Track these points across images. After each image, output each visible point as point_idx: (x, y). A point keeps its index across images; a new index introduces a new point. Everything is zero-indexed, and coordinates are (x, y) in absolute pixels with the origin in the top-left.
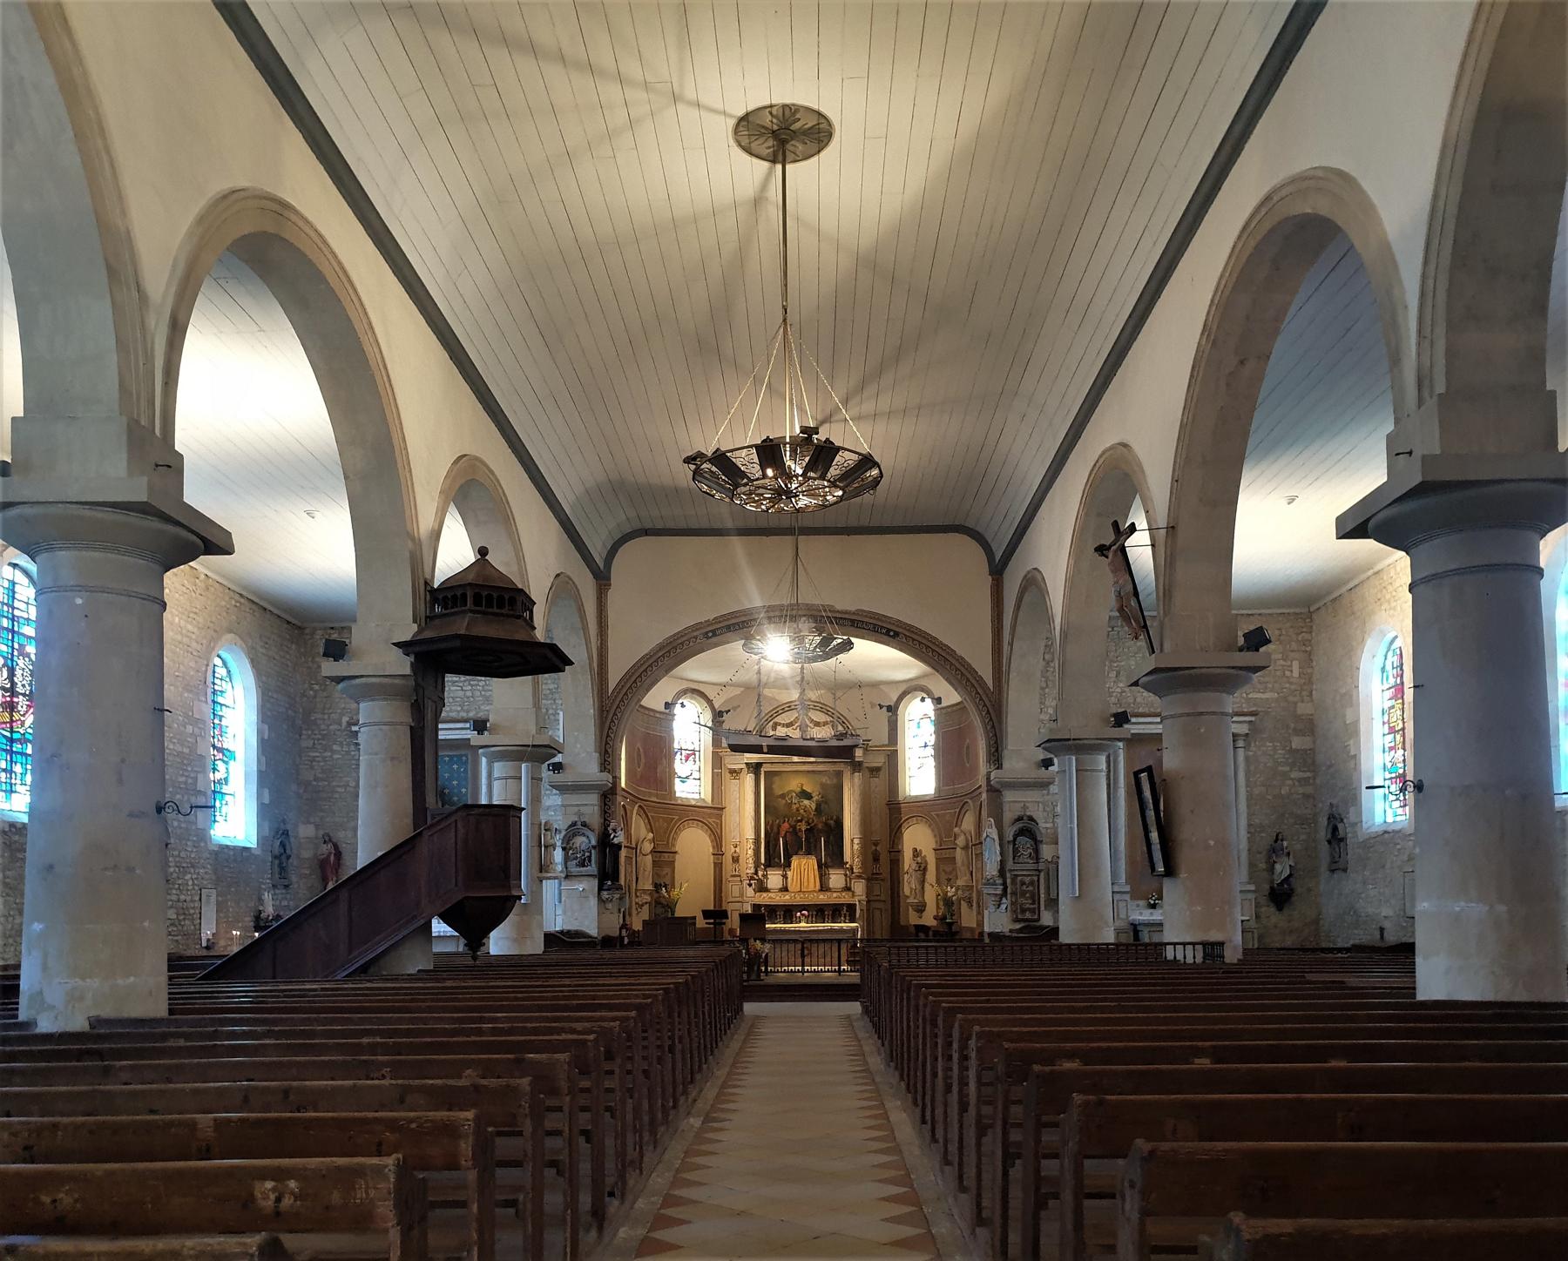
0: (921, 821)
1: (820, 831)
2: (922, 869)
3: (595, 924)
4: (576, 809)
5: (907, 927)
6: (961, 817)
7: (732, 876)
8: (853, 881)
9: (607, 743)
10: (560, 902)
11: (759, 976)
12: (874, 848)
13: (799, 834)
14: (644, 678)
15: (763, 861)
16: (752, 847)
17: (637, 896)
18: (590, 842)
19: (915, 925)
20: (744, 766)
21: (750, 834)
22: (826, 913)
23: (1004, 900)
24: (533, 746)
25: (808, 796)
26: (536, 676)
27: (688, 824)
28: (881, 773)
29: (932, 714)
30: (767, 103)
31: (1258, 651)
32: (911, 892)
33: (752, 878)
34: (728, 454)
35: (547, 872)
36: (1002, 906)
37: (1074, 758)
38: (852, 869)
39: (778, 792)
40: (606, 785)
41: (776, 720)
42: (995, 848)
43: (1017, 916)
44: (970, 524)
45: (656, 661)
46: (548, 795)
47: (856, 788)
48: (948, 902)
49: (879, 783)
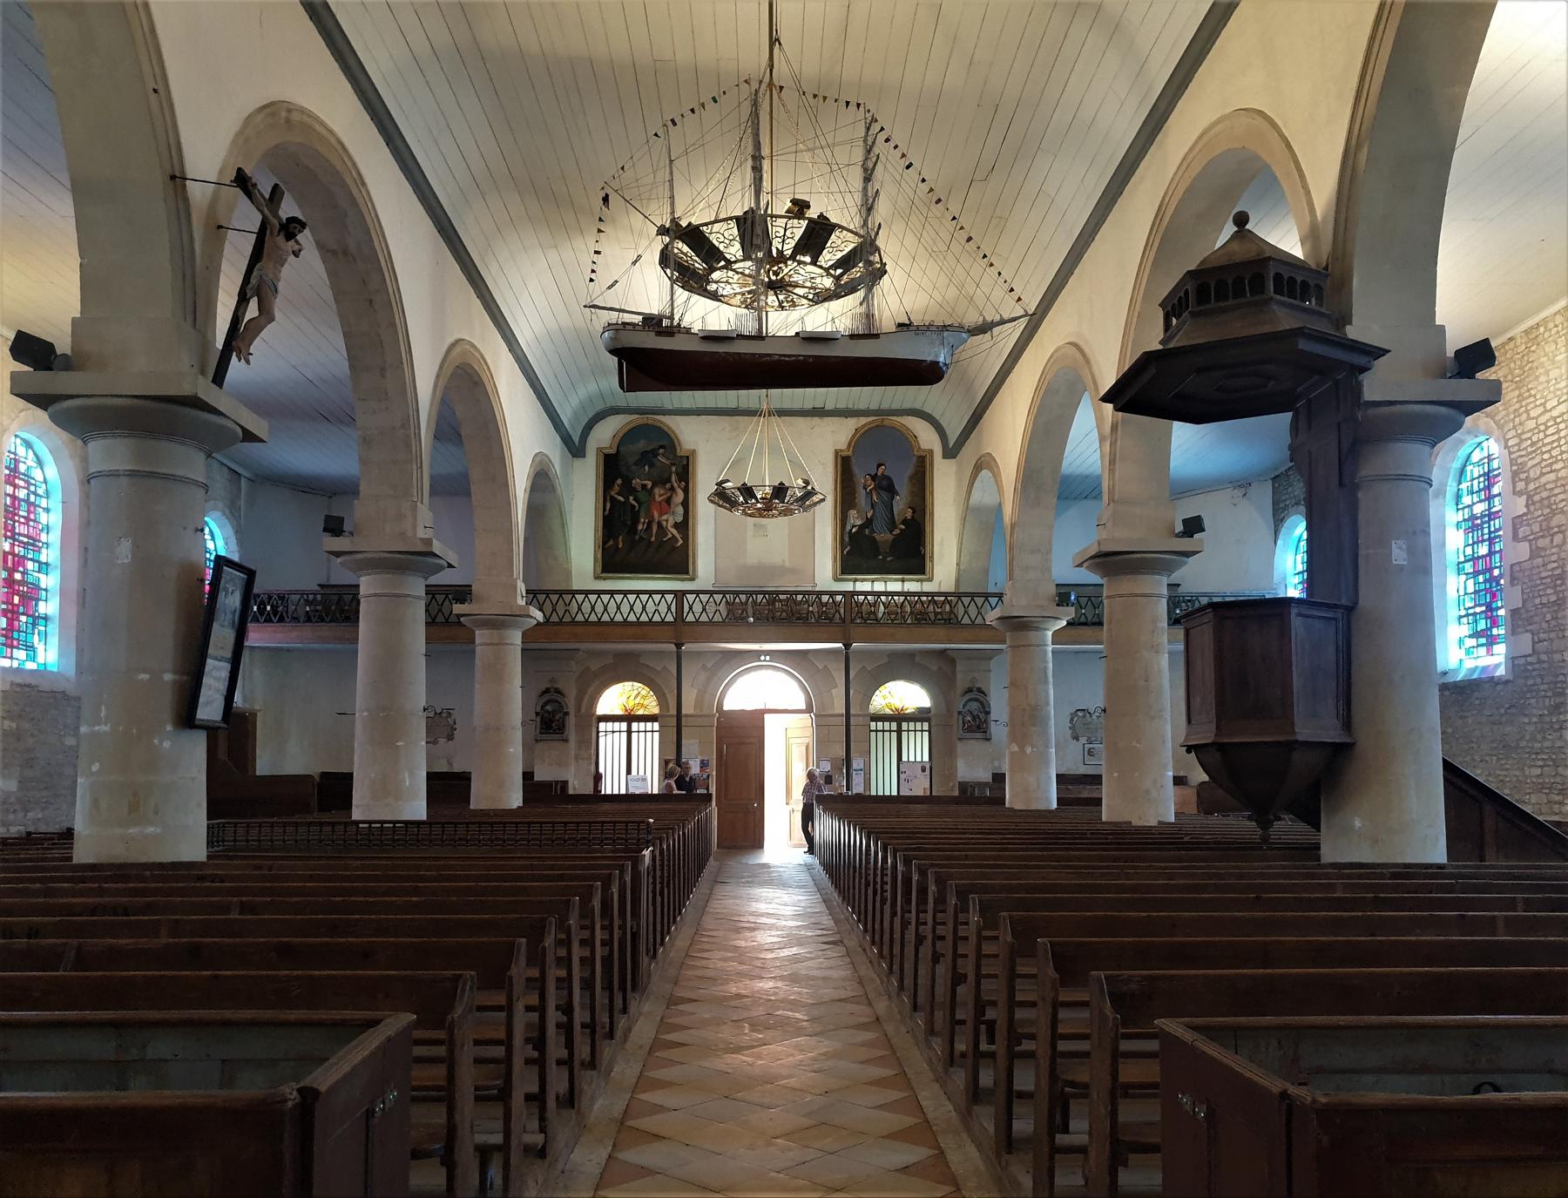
31: (1192, 537)
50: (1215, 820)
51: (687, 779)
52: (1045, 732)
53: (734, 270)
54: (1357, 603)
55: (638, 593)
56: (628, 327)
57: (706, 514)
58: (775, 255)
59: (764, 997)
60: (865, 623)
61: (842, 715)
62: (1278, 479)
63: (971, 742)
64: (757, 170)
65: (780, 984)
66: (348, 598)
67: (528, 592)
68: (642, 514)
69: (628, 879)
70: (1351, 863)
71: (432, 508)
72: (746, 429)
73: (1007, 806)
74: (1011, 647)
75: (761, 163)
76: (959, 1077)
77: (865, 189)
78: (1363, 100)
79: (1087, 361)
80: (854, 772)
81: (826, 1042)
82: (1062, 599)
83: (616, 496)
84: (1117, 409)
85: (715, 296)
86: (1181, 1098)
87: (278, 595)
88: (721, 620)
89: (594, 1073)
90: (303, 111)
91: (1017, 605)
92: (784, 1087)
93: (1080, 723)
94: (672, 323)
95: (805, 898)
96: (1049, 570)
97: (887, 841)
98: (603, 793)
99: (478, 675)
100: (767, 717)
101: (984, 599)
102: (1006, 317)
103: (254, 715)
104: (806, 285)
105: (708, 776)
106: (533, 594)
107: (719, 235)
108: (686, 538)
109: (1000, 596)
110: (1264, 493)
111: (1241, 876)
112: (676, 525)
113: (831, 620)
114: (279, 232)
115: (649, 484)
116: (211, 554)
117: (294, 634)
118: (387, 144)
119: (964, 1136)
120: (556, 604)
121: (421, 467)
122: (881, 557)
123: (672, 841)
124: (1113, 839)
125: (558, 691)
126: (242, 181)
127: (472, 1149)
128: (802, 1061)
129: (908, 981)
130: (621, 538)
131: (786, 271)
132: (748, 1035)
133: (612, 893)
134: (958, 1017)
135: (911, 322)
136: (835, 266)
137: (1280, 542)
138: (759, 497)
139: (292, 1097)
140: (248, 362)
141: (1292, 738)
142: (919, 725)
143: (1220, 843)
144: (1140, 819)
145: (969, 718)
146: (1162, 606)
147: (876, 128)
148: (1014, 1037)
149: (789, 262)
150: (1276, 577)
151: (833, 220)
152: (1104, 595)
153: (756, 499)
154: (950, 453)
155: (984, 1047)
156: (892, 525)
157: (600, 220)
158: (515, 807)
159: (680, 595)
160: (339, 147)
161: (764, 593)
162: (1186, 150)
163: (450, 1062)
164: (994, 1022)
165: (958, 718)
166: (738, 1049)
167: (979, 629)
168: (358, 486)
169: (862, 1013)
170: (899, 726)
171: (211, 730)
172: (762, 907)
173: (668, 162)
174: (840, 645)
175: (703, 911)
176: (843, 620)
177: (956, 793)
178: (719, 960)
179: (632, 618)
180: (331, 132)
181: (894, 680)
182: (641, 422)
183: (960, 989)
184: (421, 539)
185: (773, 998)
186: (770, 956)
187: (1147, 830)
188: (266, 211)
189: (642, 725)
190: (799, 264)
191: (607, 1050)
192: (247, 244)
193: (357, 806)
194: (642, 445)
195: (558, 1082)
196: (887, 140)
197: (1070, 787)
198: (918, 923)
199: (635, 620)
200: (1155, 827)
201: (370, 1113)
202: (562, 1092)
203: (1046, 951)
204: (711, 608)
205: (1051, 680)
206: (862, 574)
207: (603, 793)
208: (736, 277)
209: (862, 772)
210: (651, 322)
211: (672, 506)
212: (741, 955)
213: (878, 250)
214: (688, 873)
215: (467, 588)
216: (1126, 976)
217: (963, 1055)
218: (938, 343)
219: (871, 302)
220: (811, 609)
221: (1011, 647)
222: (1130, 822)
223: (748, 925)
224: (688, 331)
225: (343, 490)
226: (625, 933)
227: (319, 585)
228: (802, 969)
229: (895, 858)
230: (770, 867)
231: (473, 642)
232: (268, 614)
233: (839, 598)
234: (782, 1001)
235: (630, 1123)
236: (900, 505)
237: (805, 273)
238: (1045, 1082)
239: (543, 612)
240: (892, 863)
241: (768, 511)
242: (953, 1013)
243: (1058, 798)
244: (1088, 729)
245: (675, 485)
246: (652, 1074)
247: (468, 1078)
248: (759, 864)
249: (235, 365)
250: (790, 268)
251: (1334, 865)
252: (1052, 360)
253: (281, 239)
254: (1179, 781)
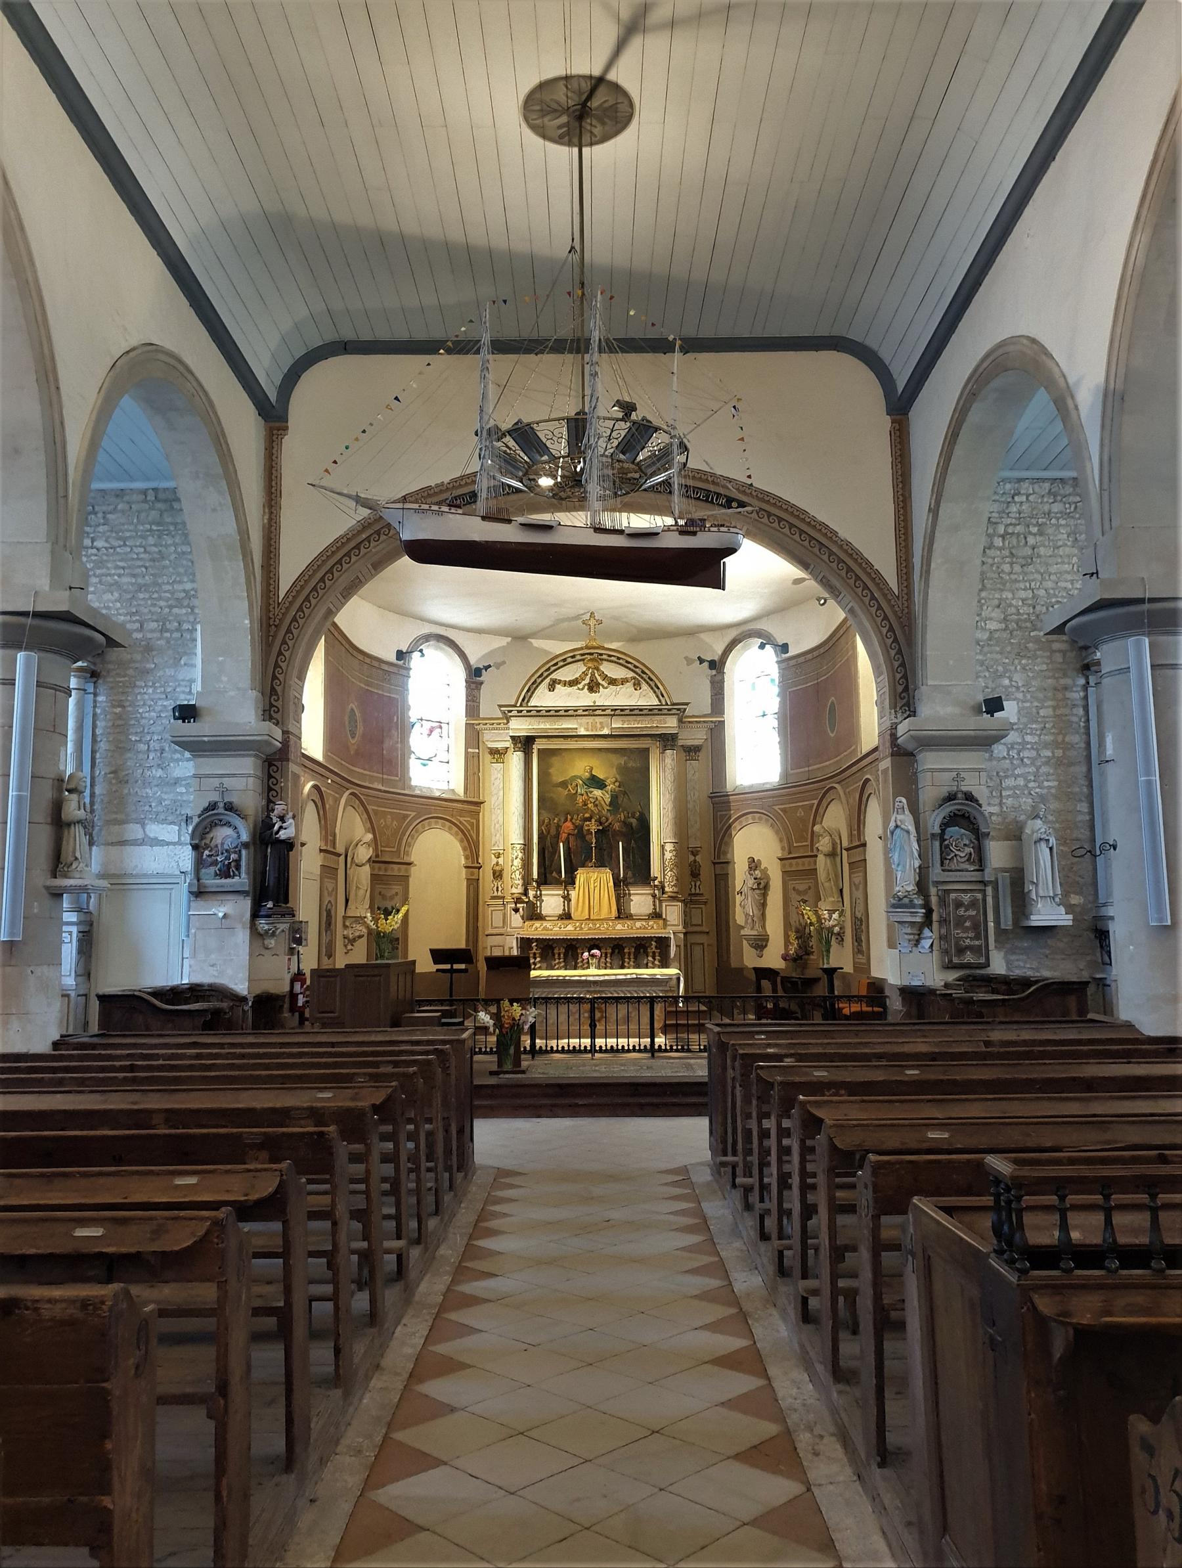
0: (760, 819)
1: (615, 833)
2: (762, 887)
3: (243, 974)
4: (216, 782)
5: (741, 970)
6: (821, 810)
7: (493, 898)
8: (664, 904)
9: (274, 677)
10: (188, 936)
11: (517, 1062)
12: (692, 858)
13: (588, 838)
14: (336, 574)
15: (535, 876)
16: (520, 855)
17: (345, 927)
18: (239, 837)
19: (755, 969)
20: (508, 744)
21: (515, 836)
22: (626, 950)
23: (927, 933)
24: (37, 615)
25: (599, 783)
27: (429, 824)
28: (702, 755)
29: (774, 671)
32: (746, 922)
33: (518, 901)
35: (66, 876)
36: (923, 941)
37: (1147, 640)
38: (663, 888)
39: (558, 778)
40: (267, 743)
41: (553, 676)
42: (910, 846)
43: (950, 961)
44: (855, 335)
45: (357, 547)
46: (178, 760)
47: (668, 772)
48: (802, 934)
49: (698, 769)
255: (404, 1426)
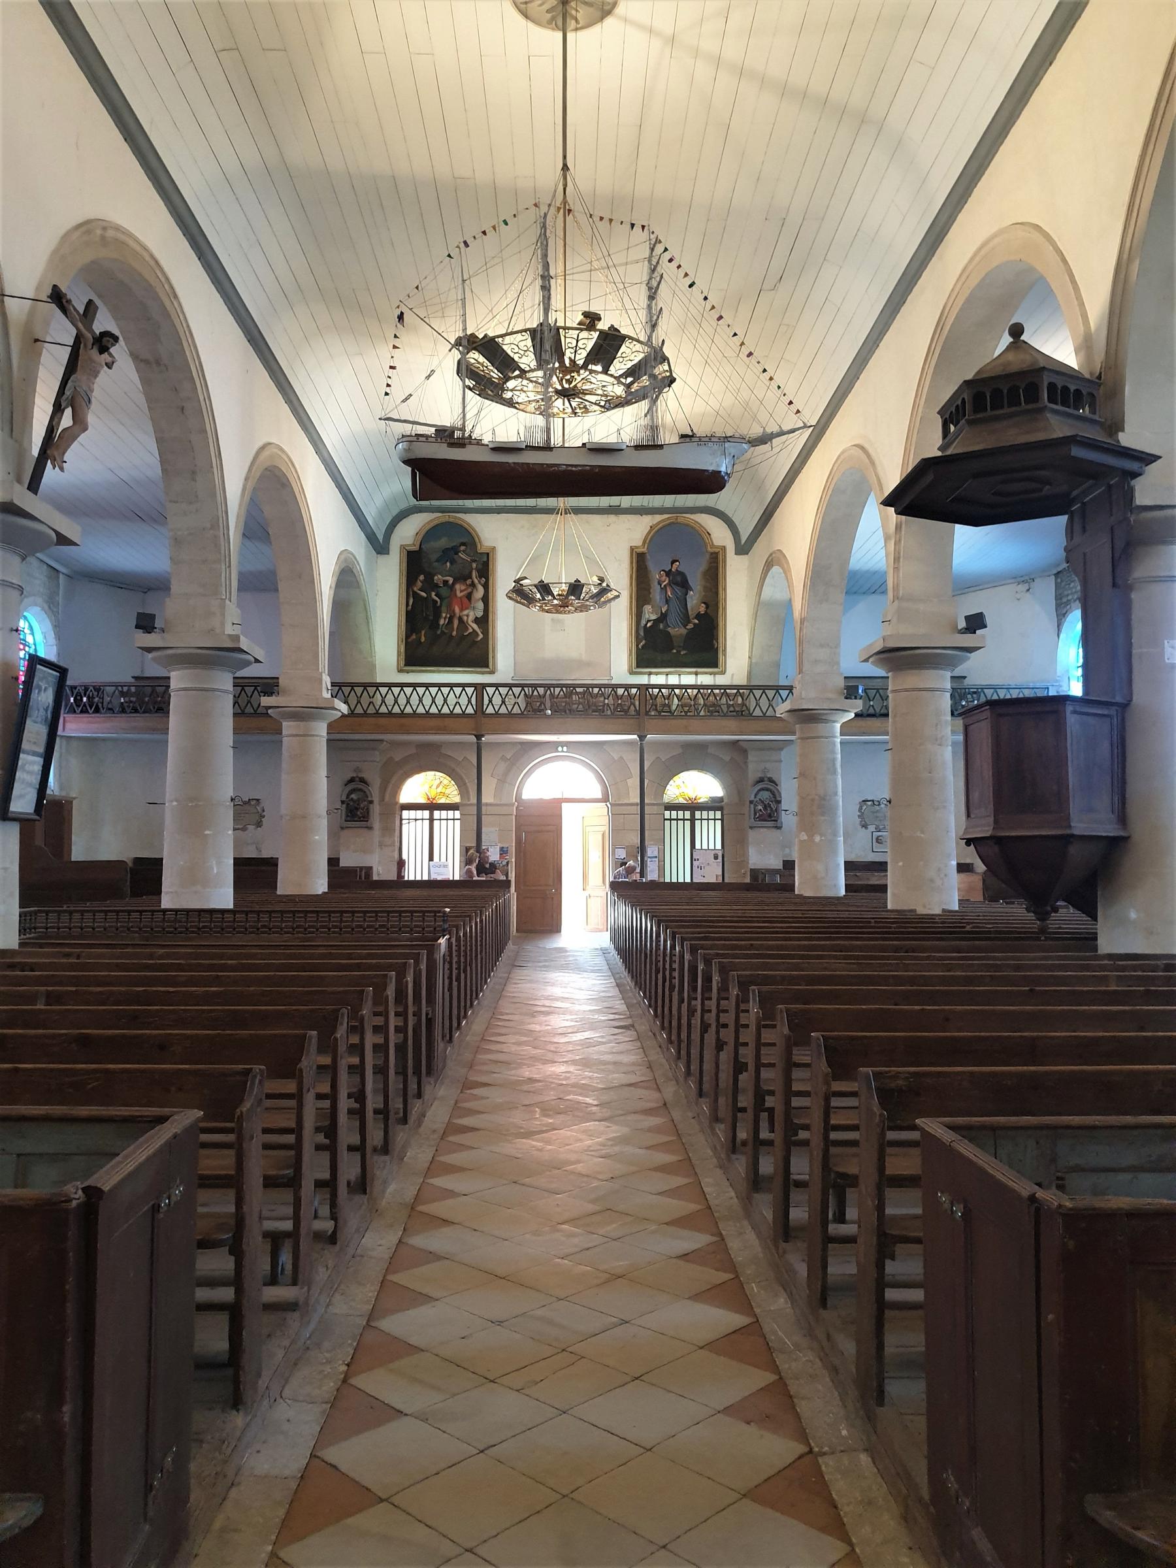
26: (566, 498)
30: (579, 33)
34: (500, 340)
50: (1000, 907)
51: (487, 866)
52: (833, 822)
53: (528, 379)
54: (1131, 700)
55: (440, 686)
56: (421, 439)
57: (505, 612)
58: (568, 365)
59: (556, 1081)
60: (660, 715)
61: (637, 804)
62: (1060, 575)
63: (762, 830)
64: (546, 289)
65: (572, 1069)
66: (160, 690)
67: (333, 684)
68: (444, 609)
69: (423, 967)
70: (1126, 954)
71: (239, 606)
72: (544, 526)
73: (796, 893)
74: (799, 738)
75: (549, 283)
76: (740, 1164)
77: (649, 307)
78: (1135, 214)
79: (873, 463)
80: (649, 860)
81: (614, 1128)
82: (850, 692)
83: (419, 592)
84: (897, 513)
85: (510, 403)
86: (940, 1197)
87: (94, 687)
88: (520, 712)
89: (387, 1158)
90: (118, 228)
91: (806, 697)
92: (572, 1172)
93: (868, 811)
94: (463, 434)
95: (602, 982)
96: (838, 663)
97: (676, 930)
98: (406, 879)
99: (284, 765)
100: (564, 805)
101: (775, 691)
102: (786, 428)
103: (70, 803)
104: (597, 393)
105: (508, 863)
106: (338, 687)
107: (513, 346)
108: (486, 633)
109: (790, 689)
110: (1046, 588)
111: (1018, 968)
112: (476, 620)
113: (626, 712)
114: (93, 345)
115: (451, 580)
116: (29, 647)
117: (108, 725)
118: (199, 259)
119: (746, 1223)
120: (361, 696)
121: (230, 566)
122: (675, 651)
123: (472, 927)
124: (897, 928)
125: (362, 780)
126: (58, 298)
127: (260, 1238)
128: (590, 1146)
129: (694, 1067)
130: (423, 632)
131: (579, 379)
132: (539, 1120)
133: (407, 982)
134: (740, 1105)
135: (694, 434)
136: (627, 374)
137: (1062, 636)
138: (555, 594)
139: (77, 1196)
140: (62, 469)
141: (1068, 832)
142: (711, 813)
143: (1000, 932)
144: (924, 906)
145: (760, 807)
146: (946, 702)
147: (659, 249)
148: (791, 1129)
149: (582, 372)
150: (1060, 669)
151: (623, 331)
152: (890, 688)
153: (553, 595)
154: (743, 549)
155: (764, 1134)
156: (686, 620)
157: (396, 336)
158: (320, 893)
159: (480, 688)
160: (152, 263)
161: (561, 686)
162: (965, 261)
163: (239, 1149)
164: (773, 1109)
165: (750, 807)
166: (529, 1134)
167: (769, 721)
168: (169, 581)
169: (650, 1098)
170: (693, 815)
171: (24, 822)
172: (557, 991)
173: (460, 282)
174: (635, 737)
175: (500, 994)
176: (638, 713)
177: (748, 880)
178: (514, 1043)
179: (434, 710)
180: (145, 249)
181: (688, 770)
182: (443, 520)
183: (743, 1077)
184: (229, 635)
185: (564, 1082)
186: (563, 1040)
187: (931, 918)
188: (80, 325)
189: (444, 813)
190: (590, 373)
191: (401, 1134)
192: (64, 354)
193: (167, 893)
194: (443, 543)
195: (349, 1169)
196: (671, 260)
197: (858, 874)
198: (703, 1011)
199: (437, 712)
200: (939, 915)
201: (156, 1208)
202: (353, 1178)
203: (819, 1046)
204: (510, 701)
205: (839, 770)
206: (656, 667)
207: (406, 879)
208: (531, 385)
209: (657, 859)
210: (444, 434)
211: (473, 601)
212: (535, 1039)
213: (665, 359)
214: (486, 959)
215: (275, 681)
216: (893, 1073)
217: (744, 1143)
218: (719, 453)
219: (655, 414)
220: (606, 701)
221: (802, 739)
222: (915, 911)
223: (543, 1009)
224: (479, 442)
225: (154, 586)
226: (420, 1020)
227: (133, 677)
228: (594, 1053)
229: (682, 947)
230: (566, 951)
231: (281, 734)
232: (85, 705)
233: (634, 691)
234: (574, 1085)
235: (421, 1208)
236: (694, 601)
237: (600, 382)
238: (818, 1170)
239: (349, 705)
240: (680, 951)
241: (564, 607)
242: (735, 1100)
243: (846, 885)
244: (877, 817)
245: (476, 581)
246: (442, 1159)
247: (257, 1166)
248: (556, 949)
249: (50, 473)
250: (582, 377)
251: (1111, 956)
252: (839, 462)
253: (94, 353)
254: (963, 868)
255: (395, 1272)
